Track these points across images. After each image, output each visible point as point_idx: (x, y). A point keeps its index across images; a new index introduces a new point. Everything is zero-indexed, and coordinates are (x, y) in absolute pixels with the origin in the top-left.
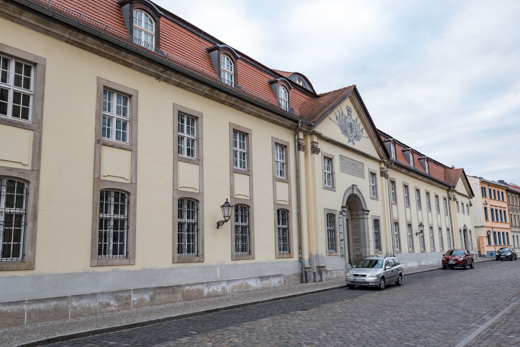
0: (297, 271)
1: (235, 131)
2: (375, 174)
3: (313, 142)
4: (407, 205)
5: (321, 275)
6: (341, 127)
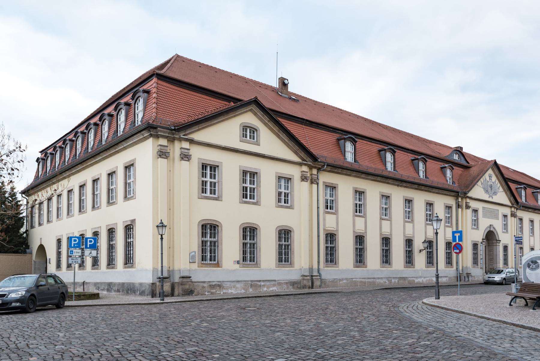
0: (455, 275)
1: (356, 191)
2: (506, 216)
3: (466, 203)
4: (532, 235)
5: (468, 278)
6: (484, 189)
